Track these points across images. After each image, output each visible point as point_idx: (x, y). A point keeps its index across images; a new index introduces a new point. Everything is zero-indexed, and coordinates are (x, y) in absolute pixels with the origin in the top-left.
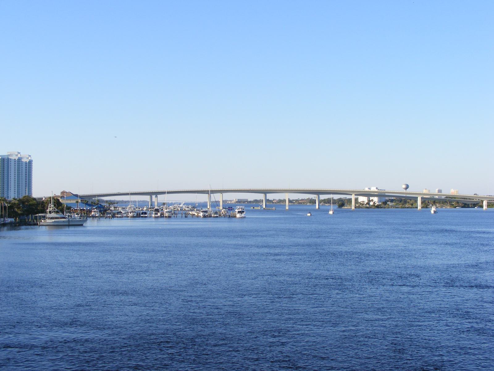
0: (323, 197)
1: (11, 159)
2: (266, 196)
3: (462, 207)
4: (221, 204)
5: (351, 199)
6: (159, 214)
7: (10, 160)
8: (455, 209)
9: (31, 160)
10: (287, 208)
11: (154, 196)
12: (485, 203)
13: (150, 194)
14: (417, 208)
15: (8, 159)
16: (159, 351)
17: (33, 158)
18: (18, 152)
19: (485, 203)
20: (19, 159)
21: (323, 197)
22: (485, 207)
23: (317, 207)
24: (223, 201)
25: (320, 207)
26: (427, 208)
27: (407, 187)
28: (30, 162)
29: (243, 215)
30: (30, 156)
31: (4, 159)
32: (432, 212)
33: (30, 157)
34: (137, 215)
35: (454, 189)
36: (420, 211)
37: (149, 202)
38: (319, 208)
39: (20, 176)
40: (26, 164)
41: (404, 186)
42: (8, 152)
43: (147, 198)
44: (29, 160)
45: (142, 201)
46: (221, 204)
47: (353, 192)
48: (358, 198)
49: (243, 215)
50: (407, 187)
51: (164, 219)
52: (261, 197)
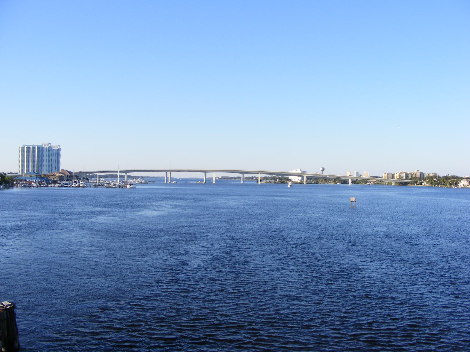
0: (246, 175)
1: (44, 148)
2: (206, 174)
3: (342, 183)
4: (214, 179)
5: (258, 178)
6: (77, 185)
7: (43, 148)
8: (336, 185)
9: (59, 148)
10: (214, 182)
11: (169, 173)
12: (350, 181)
13: (166, 171)
14: (303, 183)
15: (42, 147)
16: (467, 256)
17: (61, 147)
18: (49, 143)
19: (350, 181)
20: (50, 148)
21: (246, 175)
22: (350, 184)
23: (242, 182)
24: (215, 178)
25: (244, 182)
26: (317, 184)
27: (323, 170)
28: (59, 150)
29: (132, 186)
30: (59, 146)
31: (39, 148)
32: (289, 186)
33: (59, 147)
34: (62, 185)
35: (366, 172)
36: (305, 186)
37: (165, 177)
38: (206, 182)
39: (50, 159)
40: (47, 149)
41: (321, 169)
42: (42, 143)
43: (163, 174)
44: (49, 146)
45: (146, 177)
46: (214, 179)
47: (259, 172)
48: (288, 177)
49: (132, 186)
50: (323, 170)
51: (80, 188)
52: (240, 175)
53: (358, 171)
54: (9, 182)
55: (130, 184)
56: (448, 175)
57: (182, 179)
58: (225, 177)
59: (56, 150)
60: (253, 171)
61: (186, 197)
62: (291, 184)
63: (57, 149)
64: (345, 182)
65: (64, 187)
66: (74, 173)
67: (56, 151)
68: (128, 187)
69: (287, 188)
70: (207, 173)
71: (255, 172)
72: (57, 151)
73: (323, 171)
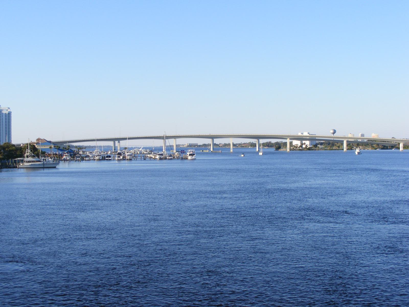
3: (382, 149)
4: (175, 148)
6: (121, 157)
8: (376, 150)
10: (232, 151)
11: (117, 142)
12: (401, 145)
13: (114, 140)
14: (343, 150)
17: (11, 110)
19: (401, 145)
22: (401, 149)
24: (176, 146)
26: (352, 150)
27: (334, 132)
28: (9, 114)
29: (193, 157)
30: (9, 108)
32: (357, 153)
36: (346, 152)
37: (112, 147)
40: (6, 115)
41: (332, 131)
43: (111, 143)
44: (9, 111)
46: (175, 148)
47: (288, 136)
49: (193, 157)
50: (334, 132)
51: (126, 161)
52: (209, 141)
53: (363, 133)
54: (277, 149)
55: (190, 155)
56: (31, 141)
57: (155, 148)
58: (196, 145)
59: (6, 113)
60: (150, 136)
61: (46, 175)
62: (360, 151)
63: (7, 112)
64: (395, 146)
65: (106, 160)
66: (16, 145)
67: (6, 115)
68: (190, 158)
69: (356, 155)
70: (214, 139)
71: (223, 137)
72: (7, 116)
73: (334, 134)
